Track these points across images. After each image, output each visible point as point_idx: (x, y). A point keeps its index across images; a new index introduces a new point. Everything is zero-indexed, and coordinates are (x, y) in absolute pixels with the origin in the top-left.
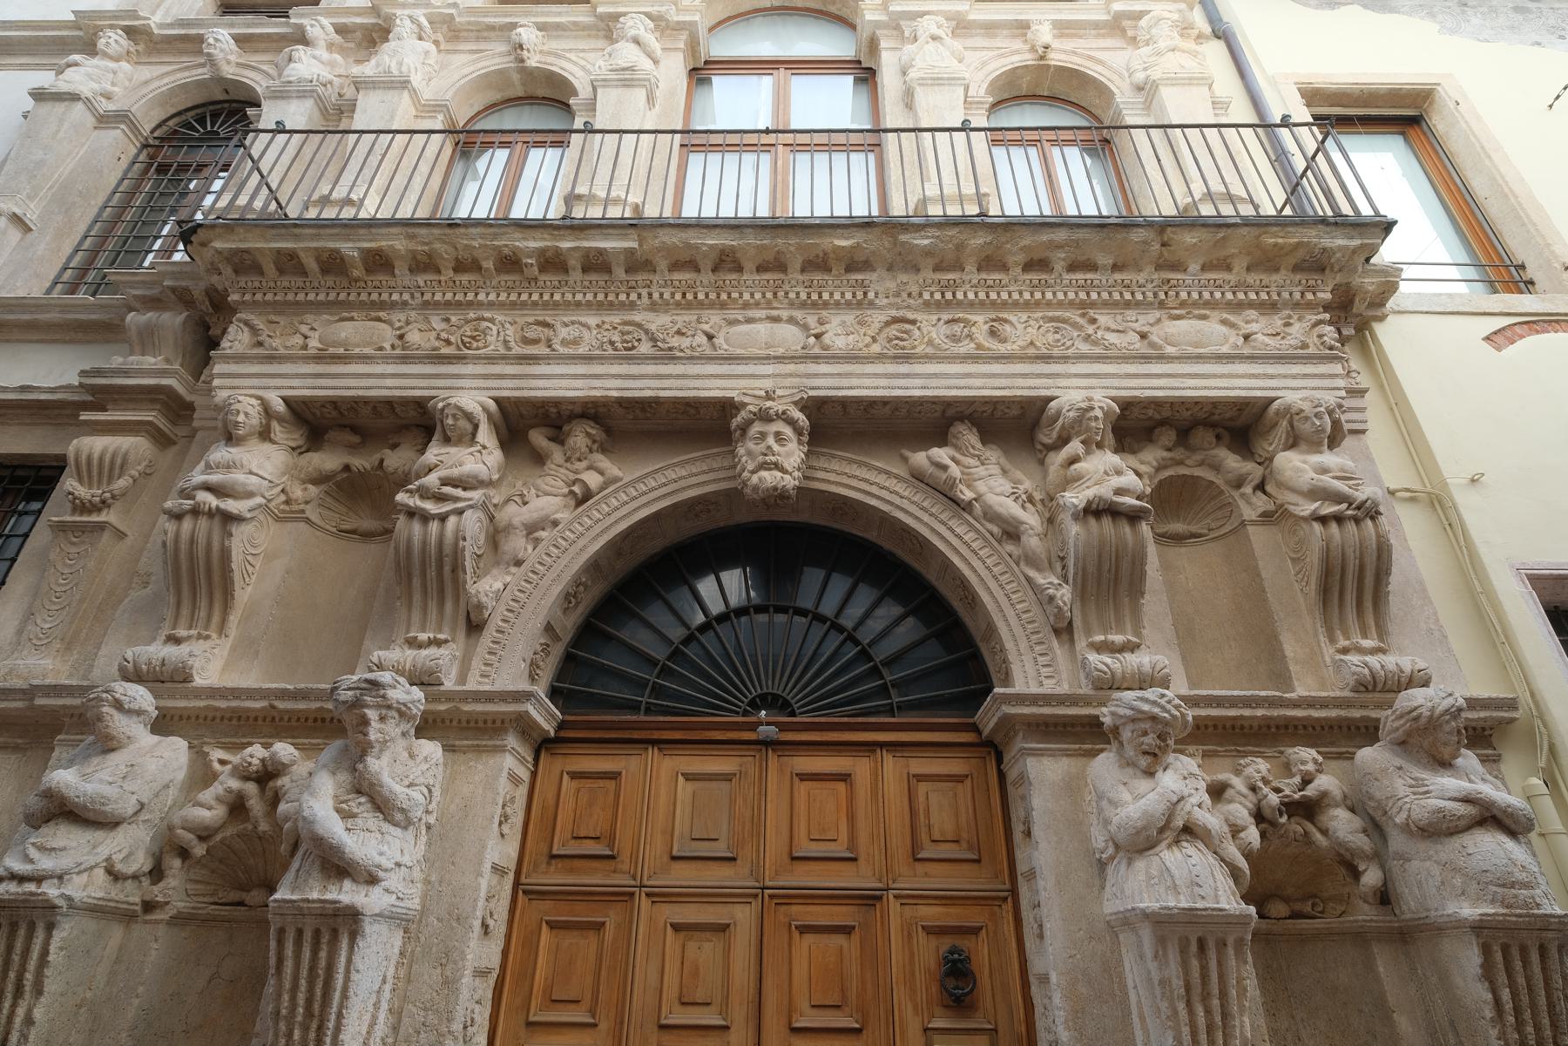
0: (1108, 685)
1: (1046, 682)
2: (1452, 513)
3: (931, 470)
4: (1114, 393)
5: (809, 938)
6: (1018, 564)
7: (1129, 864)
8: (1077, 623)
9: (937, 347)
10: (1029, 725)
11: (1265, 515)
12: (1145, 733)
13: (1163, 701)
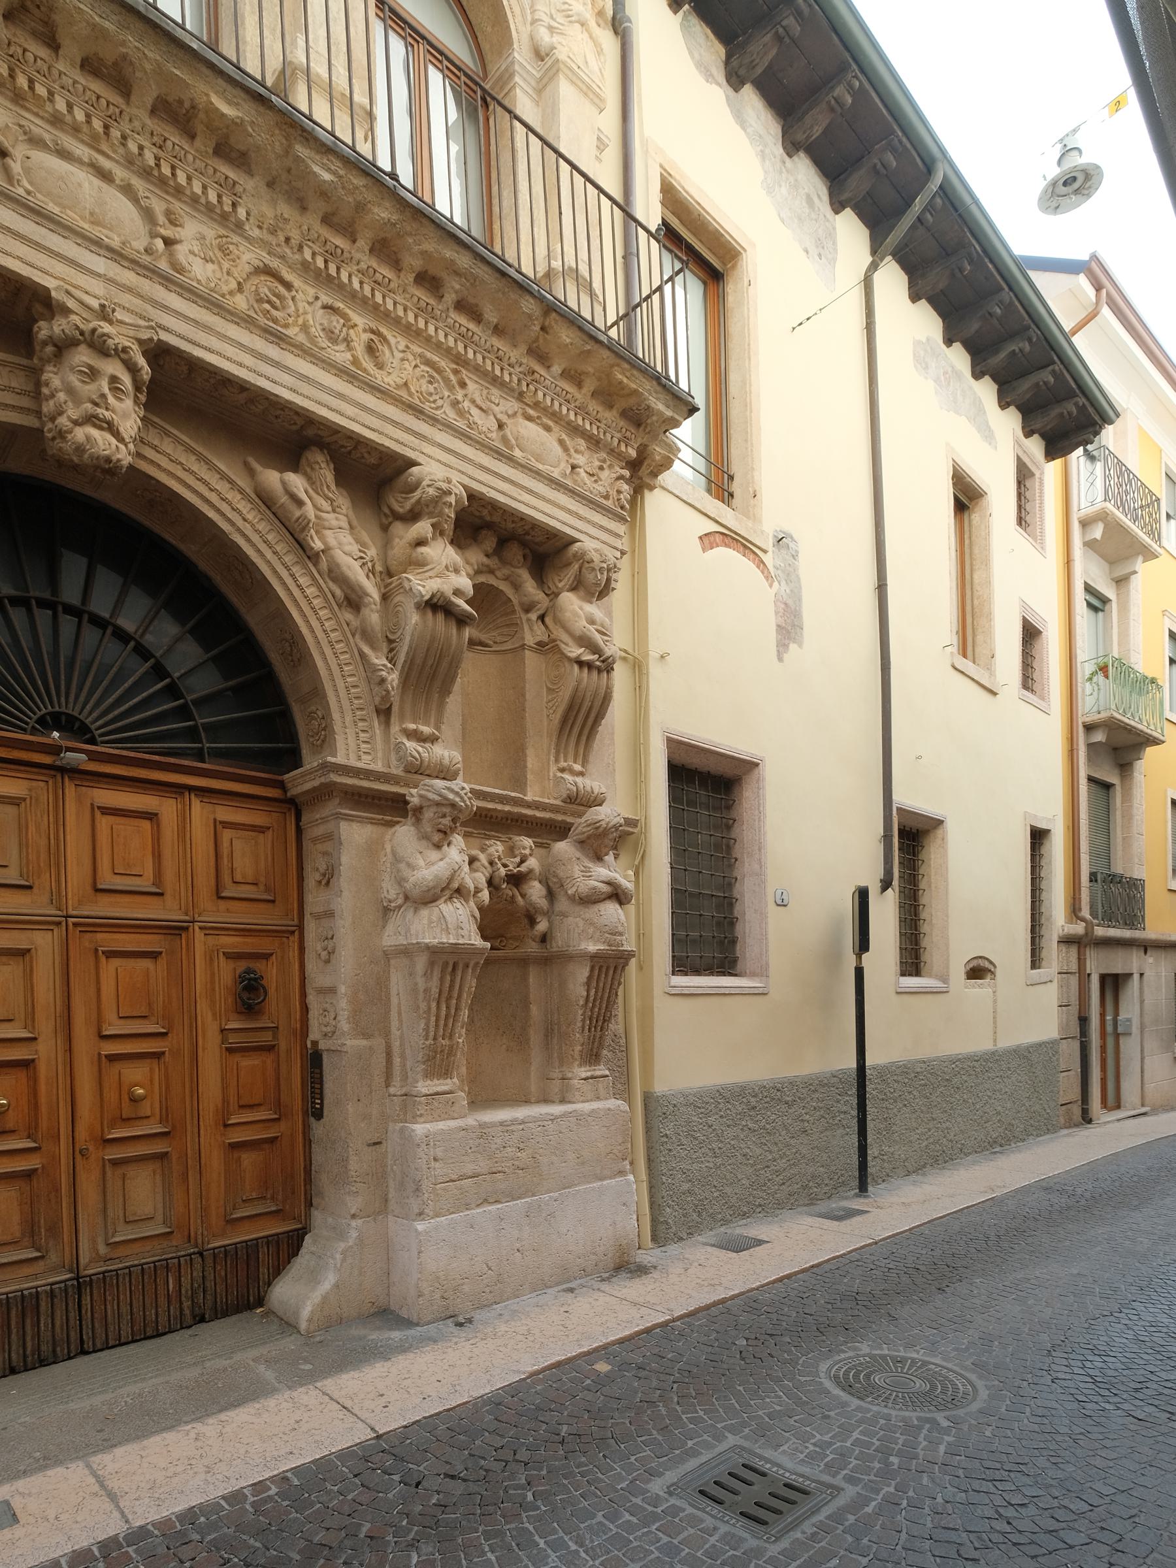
0: (417, 770)
1: (364, 757)
2: (645, 677)
3: (284, 499)
4: (467, 481)
5: (116, 962)
6: (353, 635)
7: (415, 912)
8: (395, 709)
9: (312, 339)
10: (346, 793)
11: (540, 644)
12: (444, 816)
13: (462, 793)
